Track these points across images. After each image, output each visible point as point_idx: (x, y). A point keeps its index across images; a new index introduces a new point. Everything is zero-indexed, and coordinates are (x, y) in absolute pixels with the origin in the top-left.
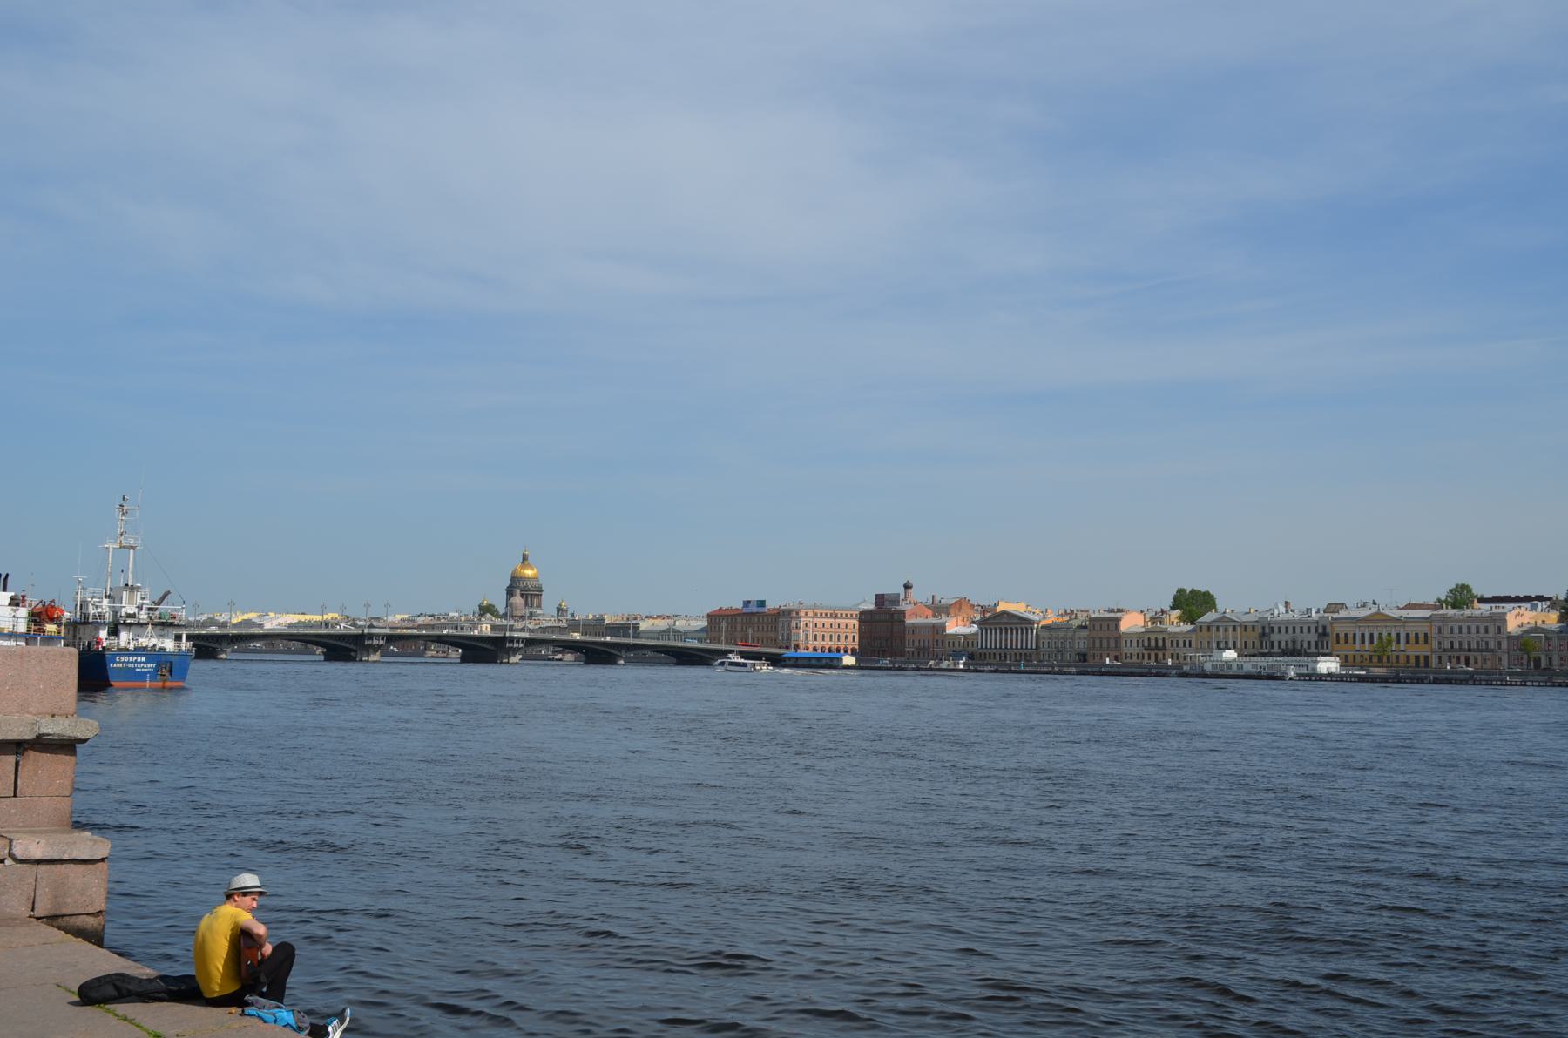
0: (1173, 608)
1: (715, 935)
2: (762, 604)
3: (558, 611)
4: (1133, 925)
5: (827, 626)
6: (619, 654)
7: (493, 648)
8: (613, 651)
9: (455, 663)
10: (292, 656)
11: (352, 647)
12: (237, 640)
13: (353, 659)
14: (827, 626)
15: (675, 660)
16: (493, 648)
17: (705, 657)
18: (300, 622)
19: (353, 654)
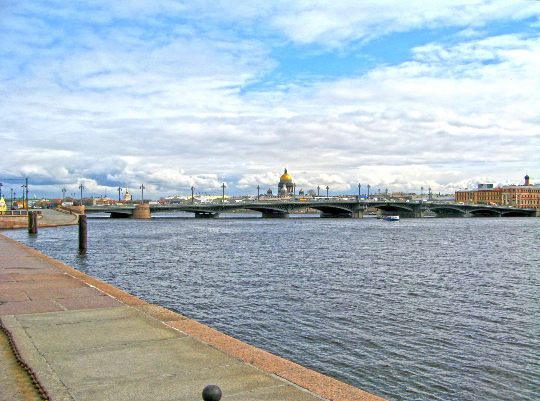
0: (351, 185)
1: (424, 353)
2: (491, 186)
3: (300, 193)
4: (387, 341)
5: (527, 196)
6: (464, 212)
7: (411, 210)
8: (283, 210)
9: (259, 218)
10: (245, 214)
11: (350, 210)
12: (297, 207)
13: (350, 217)
14: (527, 196)
15: (435, 215)
16: (411, 210)
17: (281, 212)
18: (217, 199)
19: (350, 214)
